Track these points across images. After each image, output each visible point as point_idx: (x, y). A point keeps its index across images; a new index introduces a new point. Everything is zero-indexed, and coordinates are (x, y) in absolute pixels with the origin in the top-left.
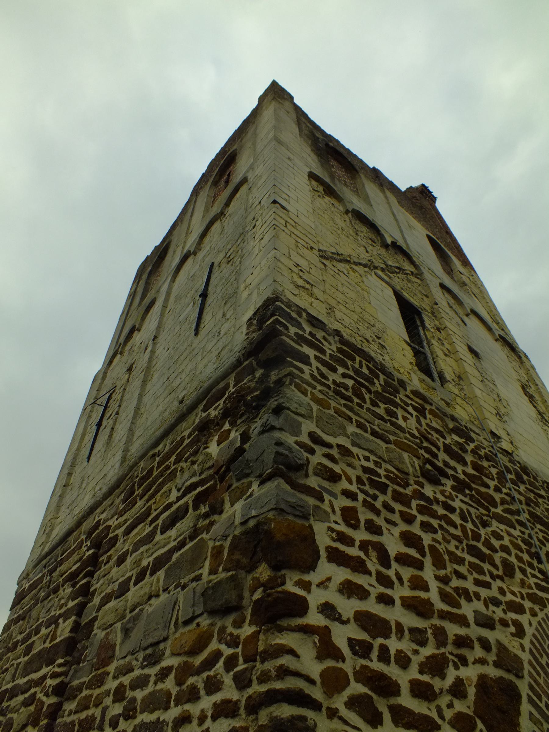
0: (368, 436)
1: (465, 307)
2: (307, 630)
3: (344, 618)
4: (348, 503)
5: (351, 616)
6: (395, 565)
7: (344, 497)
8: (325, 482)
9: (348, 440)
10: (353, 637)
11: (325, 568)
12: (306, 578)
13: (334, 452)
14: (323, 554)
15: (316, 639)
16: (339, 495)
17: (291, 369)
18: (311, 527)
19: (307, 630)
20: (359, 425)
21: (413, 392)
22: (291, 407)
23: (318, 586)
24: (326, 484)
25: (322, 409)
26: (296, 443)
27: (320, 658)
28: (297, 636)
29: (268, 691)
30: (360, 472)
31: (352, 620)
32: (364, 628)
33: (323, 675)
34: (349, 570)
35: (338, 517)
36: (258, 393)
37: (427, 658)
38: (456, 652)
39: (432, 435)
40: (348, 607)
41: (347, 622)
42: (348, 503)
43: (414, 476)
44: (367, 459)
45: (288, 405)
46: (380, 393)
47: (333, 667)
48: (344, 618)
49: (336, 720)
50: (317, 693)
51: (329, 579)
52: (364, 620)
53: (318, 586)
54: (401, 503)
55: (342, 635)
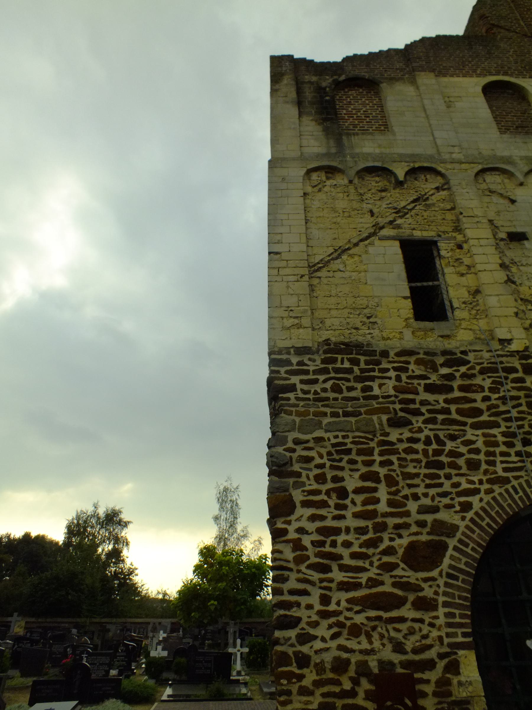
0: (342, 419)
1: (517, 177)
2: (288, 541)
3: (310, 532)
4: (318, 471)
5: (314, 530)
6: (351, 496)
7: (316, 469)
8: (304, 464)
9: (322, 430)
10: (313, 539)
11: (300, 511)
12: (289, 519)
13: (311, 444)
14: (298, 505)
15: (291, 544)
16: (313, 468)
17: (281, 402)
18: (290, 495)
19: (288, 541)
20: (335, 415)
21: (398, 354)
22: (279, 430)
23: (296, 520)
24: (305, 465)
25: (303, 418)
26: (284, 450)
27: (294, 551)
28: (283, 544)
29: (327, 573)
30: (330, 448)
31: (314, 532)
32: (321, 534)
33: (294, 558)
34: (314, 509)
35: (313, 482)
36: (8, 641)
37: (364, 541)
38: (395, 532)
39: (413, 384)
40: (311, 527)
41: (312, 533)
42: (318, 471)
43: (381, 430)
44: (336, 437)
45: (277, 430)
46: (360, 376)
47: (300, 555)
48: (310, 532)
49: (301, 574)
50: (291, 565)
51: (302, 516)
52: (324, 531)
53: (296, 520)
54: (364, 455)
55: (306, 541)
